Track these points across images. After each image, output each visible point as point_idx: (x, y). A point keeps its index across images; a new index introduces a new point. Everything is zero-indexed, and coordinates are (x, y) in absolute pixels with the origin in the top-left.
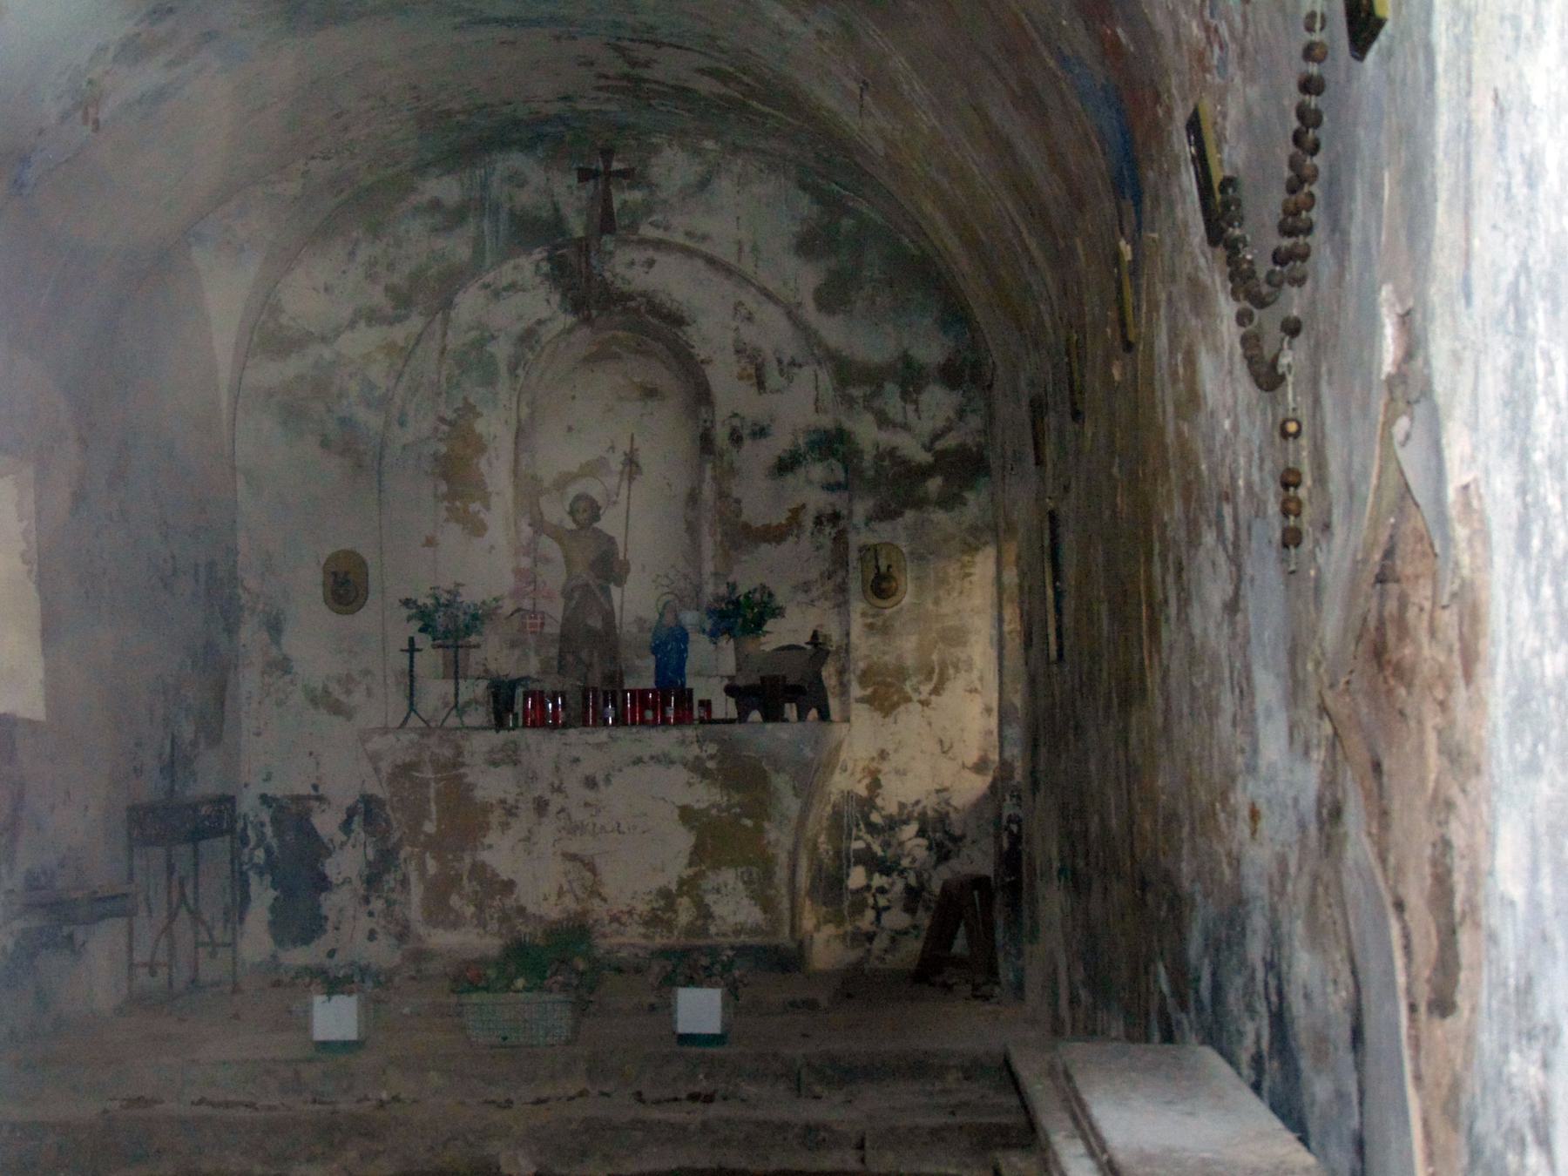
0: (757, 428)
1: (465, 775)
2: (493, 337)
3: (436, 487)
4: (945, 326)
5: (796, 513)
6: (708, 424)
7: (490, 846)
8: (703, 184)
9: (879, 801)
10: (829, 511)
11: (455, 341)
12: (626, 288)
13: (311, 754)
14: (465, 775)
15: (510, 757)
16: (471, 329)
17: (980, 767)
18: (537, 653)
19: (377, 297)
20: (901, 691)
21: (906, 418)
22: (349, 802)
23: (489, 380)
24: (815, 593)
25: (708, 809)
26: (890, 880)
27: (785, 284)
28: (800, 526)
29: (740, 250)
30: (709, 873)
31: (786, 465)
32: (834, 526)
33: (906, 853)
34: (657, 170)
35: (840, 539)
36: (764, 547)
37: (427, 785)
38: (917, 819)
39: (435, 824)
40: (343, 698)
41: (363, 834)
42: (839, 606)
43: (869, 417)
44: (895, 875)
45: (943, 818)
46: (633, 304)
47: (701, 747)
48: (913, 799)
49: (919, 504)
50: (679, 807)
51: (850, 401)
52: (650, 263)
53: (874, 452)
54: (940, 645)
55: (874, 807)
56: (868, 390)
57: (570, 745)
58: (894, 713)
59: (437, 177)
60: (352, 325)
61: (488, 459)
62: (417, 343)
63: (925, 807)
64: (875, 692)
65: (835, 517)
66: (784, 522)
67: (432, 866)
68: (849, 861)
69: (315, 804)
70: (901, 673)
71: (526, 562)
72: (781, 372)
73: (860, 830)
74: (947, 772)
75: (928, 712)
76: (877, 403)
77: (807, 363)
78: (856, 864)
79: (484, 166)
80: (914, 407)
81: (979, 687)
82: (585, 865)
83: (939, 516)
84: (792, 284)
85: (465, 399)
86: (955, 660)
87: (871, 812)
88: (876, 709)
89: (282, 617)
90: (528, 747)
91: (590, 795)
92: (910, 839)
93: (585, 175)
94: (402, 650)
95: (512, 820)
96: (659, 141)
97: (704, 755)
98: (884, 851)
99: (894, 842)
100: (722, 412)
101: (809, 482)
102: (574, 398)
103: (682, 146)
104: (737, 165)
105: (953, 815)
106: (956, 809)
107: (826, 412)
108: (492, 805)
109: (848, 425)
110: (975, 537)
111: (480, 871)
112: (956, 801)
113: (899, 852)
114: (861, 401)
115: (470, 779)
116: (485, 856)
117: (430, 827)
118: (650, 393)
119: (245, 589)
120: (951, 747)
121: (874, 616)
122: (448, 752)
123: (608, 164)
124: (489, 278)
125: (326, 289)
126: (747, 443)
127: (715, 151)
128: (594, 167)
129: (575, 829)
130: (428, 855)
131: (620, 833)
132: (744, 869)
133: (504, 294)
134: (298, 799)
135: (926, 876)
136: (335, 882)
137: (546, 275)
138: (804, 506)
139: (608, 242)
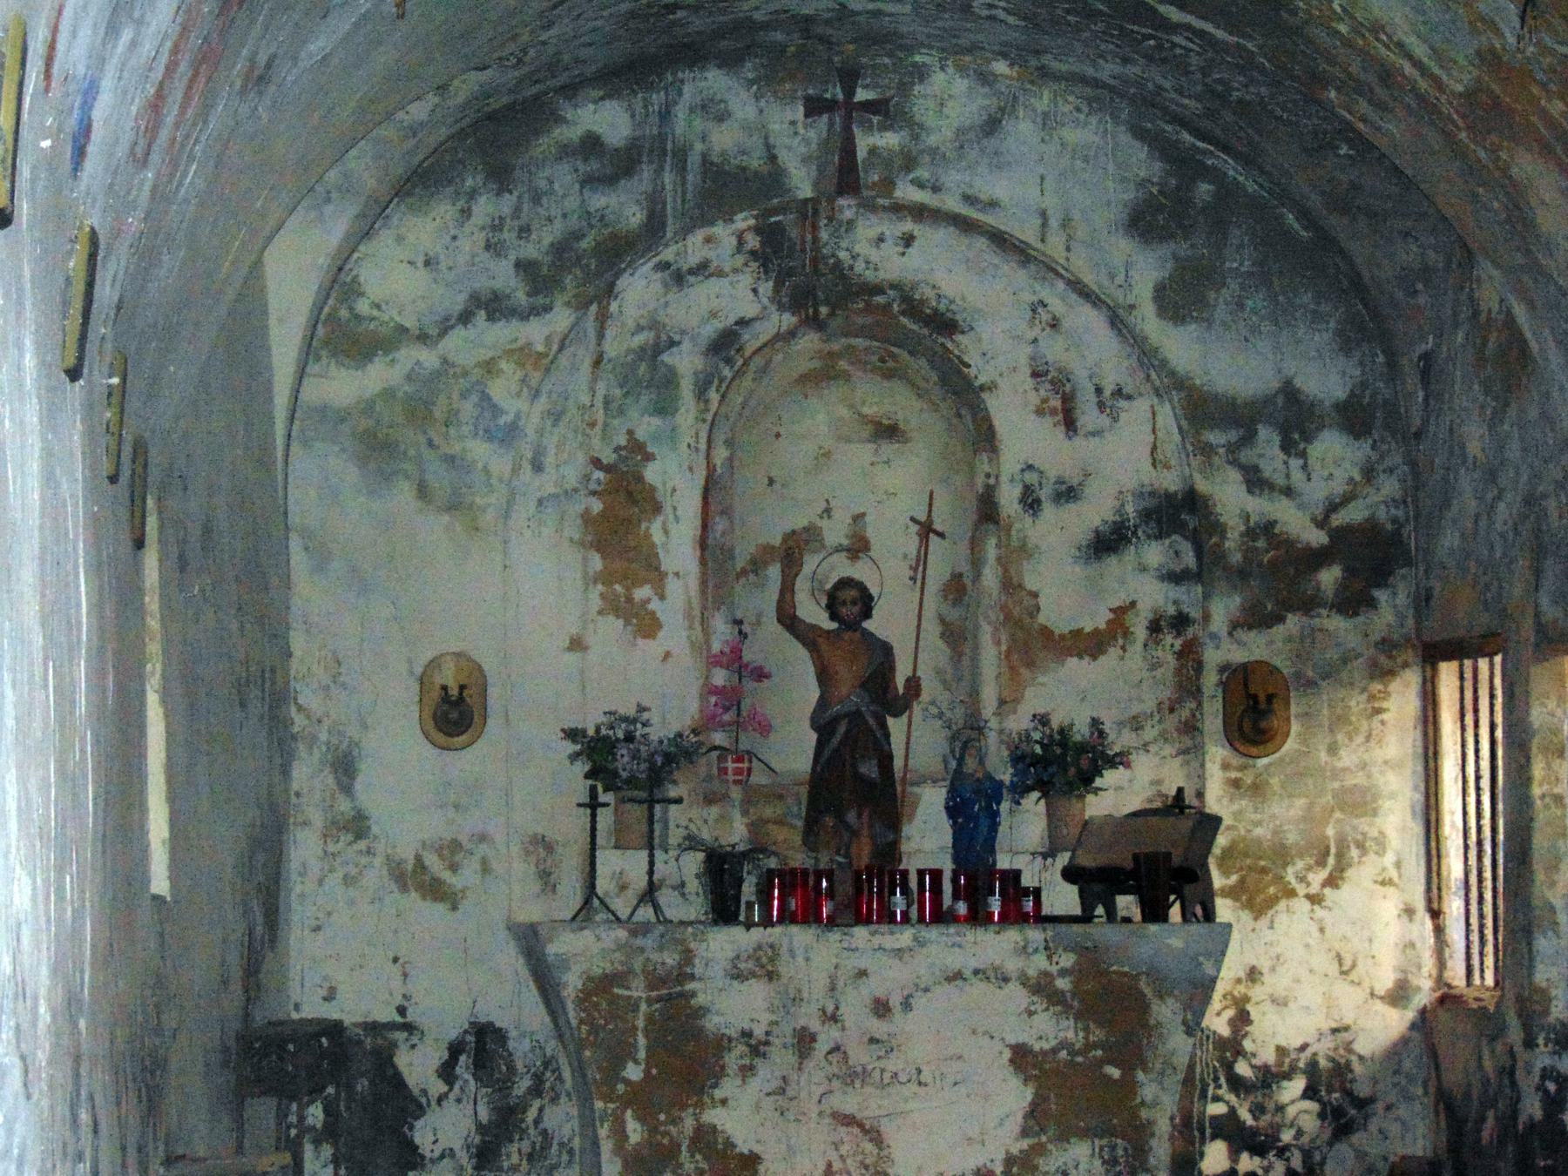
0: (1064, 487)
1: (693, 994)
2: (672, 344)
3: (585, 559)
4: (1346, 344)
5: (1120, 612)
6: (992, 481)
7: (724, 1102)
8: (992, 125)
9: (1248, 1045)
10: (1171, 610)
11: (614, 347)
12: (870, 275)
13: (396, 960)
14: (693, 994)
15: (764, 967)
16: (640, 329)
17: (1399, 995)
18: (745, 813)
19: (503, 276)
20: (1279, 879)
21: (1288, 476)
22: (453, 1034)
23: (665, 408)
24: (1149, 733)
25: (1055, 1051)
26: (1266, 1163)
27: (1112, 277)
28: (1127, 634)
29: (1044, 225)
30: (1050, 1146)
31: (1107, 543)
32: (1179, 634)
33: (1287, 1121)
34: (922, 104)
35: (1189, 655)
36: (1073, 662)
37: (636, 1008)
38: (1304, 1072)
39: (643, 1066)
40: (446, 875)
41: (472, 1082)
42: (1185, 752)
43: (1235, 475)
44: (1271, 1155)
45: (1341, 1070)
46: (880, 299)
47: (1049, 957)
48: (1298, 1043)
49: (1308, 605)
50: (1011, 1047)
51: (1207, 450)
52: (908, 240)
53: (1243, 528)
54: (1338, 815)
55: (1239, 1052)
56: (1233, 435)
57: (856, 949)
58: (1271, 913)
59: (595, 102)
60: (465, 318)
61: (664, 523)
62: (561, 348)
63: (1315, 1054)
64: (1242, 881)
65: (1181, 622)
66: (1103, 626)
67: (635, 1131)
68: (1202, 1133)
69: (400, 1036)
70: (1282, 855)
71: (720, 677)
72: (1101, 406)
73: (1220, 1087)
74: (1349, 1004)
75: (1319, 912)
76: (1246, 456)
77: (1141, 395)
78: (1214, 1137)
79: (666, 89)
80: (1301, 462)
81: (1396, 879)
82: (865, 1131)
83: (1336, 623)
84: (1120, 279)
85: (630, 433)
86: (1359, 837)
87: (1235, 1061)
88: (1243, 907)
89: (355, 753)
90: (791, 952)
91: (878, 1027)
92: (1293, 1102)
93: (814, 107)
94: (579, 805)
95: (758, 1061)
96: (927, 59)
97: (1054, 969)
98: (1255, 1118)
99: (1271, 1106)
100: (1011, 458)
101: (1143, 569)
102: (778, 435)
103: (962, 69)
104: (1043, 100)
105: (1358, 1068)
106: (1361, 1058)
107: (1167, 467)
108: (730, 1040)
109: (1202, 486)
110: (1390, 657)
111: (705, 1138)
112: (1364, 1046)
113: (1278, 1119)
114: (1221, 451)
115: (701, 999)
116: (713, 1116)
117: (634, 1072)
118: (887, 432)
119: (300, 708)
120: (1354, 966)
121: (1242, 768)
122: (670, 959)
123: (849, 93)
124: (668, 254)
125: (427, 263)
126: (1048, 510)
127: (1012, 78)
128: (828, 96)
129: (853, 1077)
130: (629, 1113)
131: (920, 1083)
132: (1105, 1142)
133: (692, 279)
134: (373, 1028)
135: (1317, 1157)
136: (428, 1155)
137: (753, 253)
138: (1133, 604)
139: (847, 207)
